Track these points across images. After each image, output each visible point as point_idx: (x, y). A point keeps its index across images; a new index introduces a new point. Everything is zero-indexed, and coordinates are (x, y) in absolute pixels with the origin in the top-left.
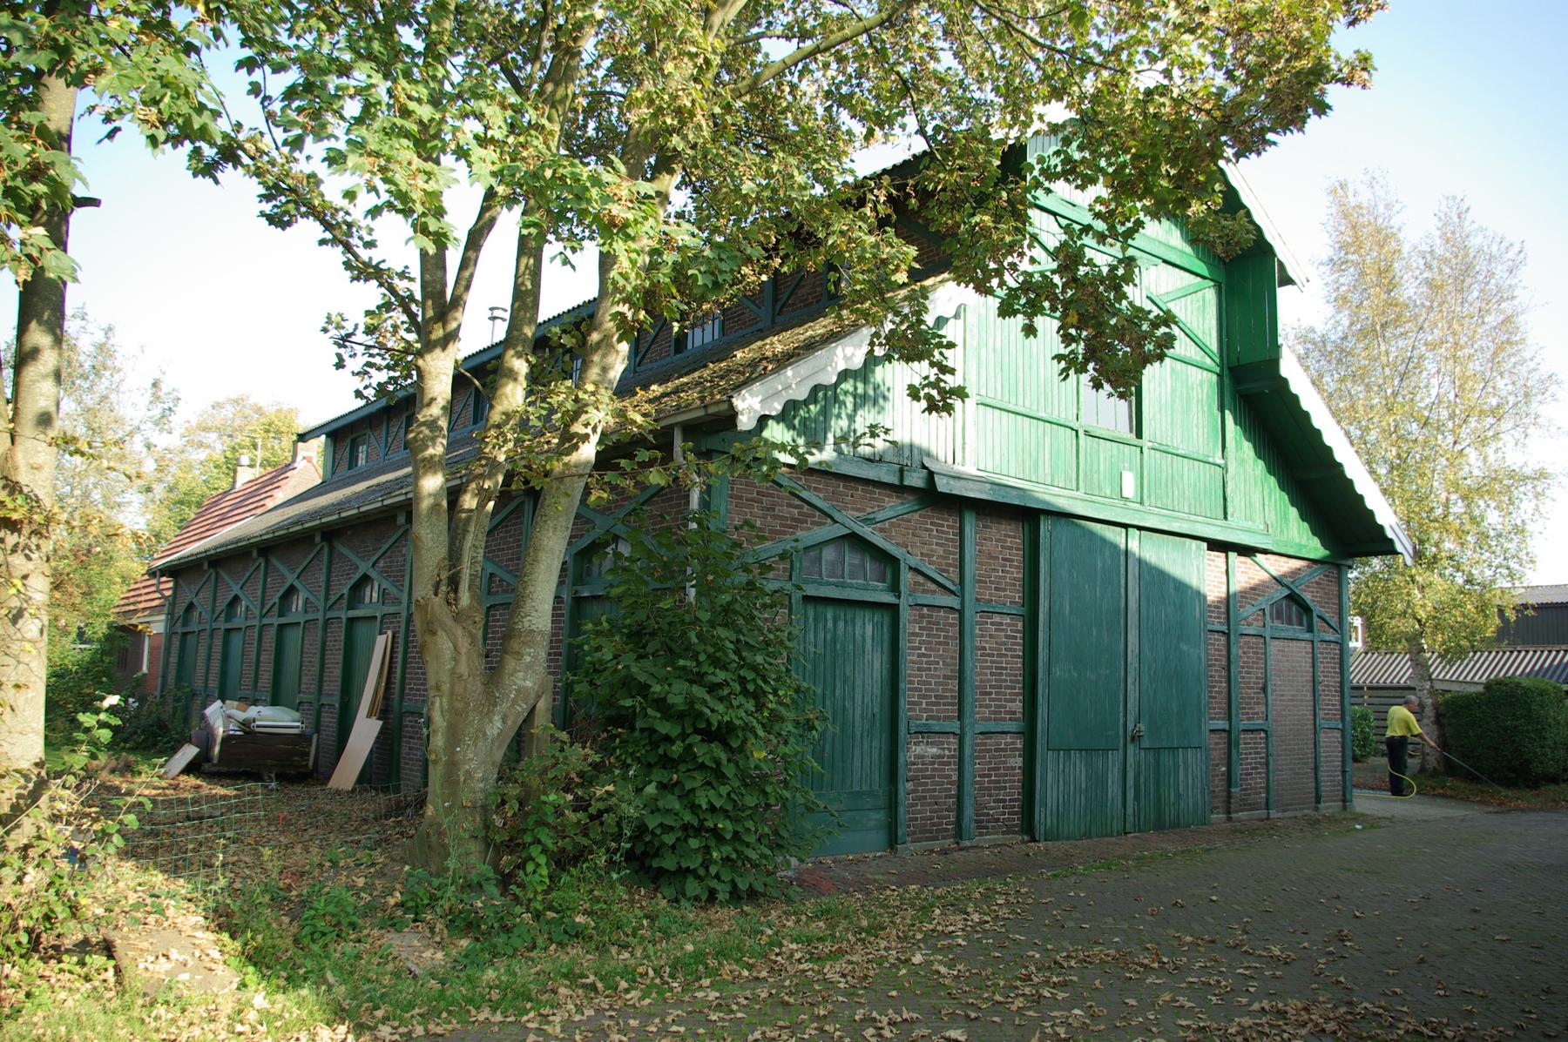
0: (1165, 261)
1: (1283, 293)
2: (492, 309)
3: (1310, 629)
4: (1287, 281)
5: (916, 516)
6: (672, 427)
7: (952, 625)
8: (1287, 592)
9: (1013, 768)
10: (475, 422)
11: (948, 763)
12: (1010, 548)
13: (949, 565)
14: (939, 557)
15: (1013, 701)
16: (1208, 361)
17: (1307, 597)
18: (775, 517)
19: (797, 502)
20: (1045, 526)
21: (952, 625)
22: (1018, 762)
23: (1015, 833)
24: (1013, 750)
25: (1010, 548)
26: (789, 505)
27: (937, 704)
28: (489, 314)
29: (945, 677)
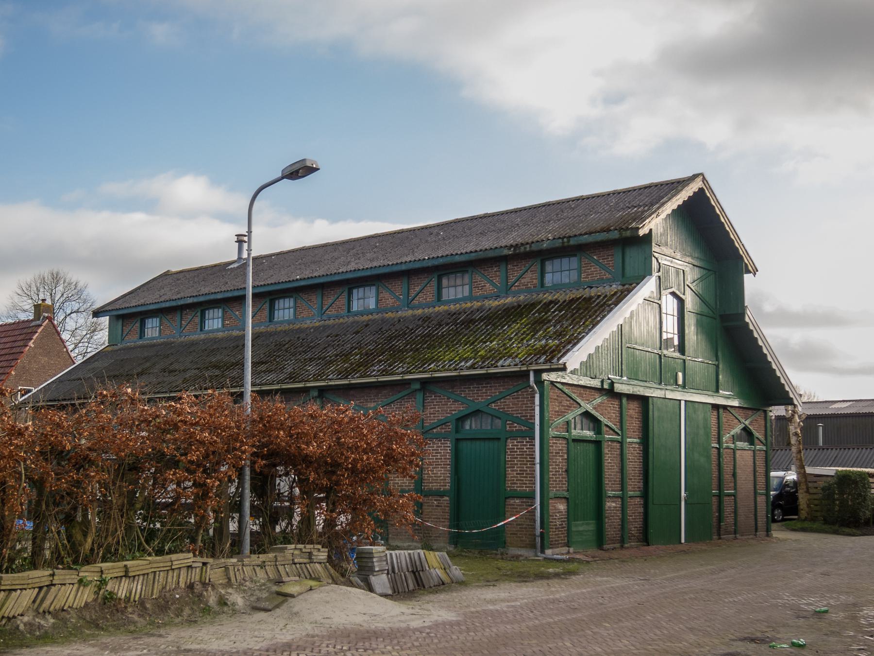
1: (747, 278)
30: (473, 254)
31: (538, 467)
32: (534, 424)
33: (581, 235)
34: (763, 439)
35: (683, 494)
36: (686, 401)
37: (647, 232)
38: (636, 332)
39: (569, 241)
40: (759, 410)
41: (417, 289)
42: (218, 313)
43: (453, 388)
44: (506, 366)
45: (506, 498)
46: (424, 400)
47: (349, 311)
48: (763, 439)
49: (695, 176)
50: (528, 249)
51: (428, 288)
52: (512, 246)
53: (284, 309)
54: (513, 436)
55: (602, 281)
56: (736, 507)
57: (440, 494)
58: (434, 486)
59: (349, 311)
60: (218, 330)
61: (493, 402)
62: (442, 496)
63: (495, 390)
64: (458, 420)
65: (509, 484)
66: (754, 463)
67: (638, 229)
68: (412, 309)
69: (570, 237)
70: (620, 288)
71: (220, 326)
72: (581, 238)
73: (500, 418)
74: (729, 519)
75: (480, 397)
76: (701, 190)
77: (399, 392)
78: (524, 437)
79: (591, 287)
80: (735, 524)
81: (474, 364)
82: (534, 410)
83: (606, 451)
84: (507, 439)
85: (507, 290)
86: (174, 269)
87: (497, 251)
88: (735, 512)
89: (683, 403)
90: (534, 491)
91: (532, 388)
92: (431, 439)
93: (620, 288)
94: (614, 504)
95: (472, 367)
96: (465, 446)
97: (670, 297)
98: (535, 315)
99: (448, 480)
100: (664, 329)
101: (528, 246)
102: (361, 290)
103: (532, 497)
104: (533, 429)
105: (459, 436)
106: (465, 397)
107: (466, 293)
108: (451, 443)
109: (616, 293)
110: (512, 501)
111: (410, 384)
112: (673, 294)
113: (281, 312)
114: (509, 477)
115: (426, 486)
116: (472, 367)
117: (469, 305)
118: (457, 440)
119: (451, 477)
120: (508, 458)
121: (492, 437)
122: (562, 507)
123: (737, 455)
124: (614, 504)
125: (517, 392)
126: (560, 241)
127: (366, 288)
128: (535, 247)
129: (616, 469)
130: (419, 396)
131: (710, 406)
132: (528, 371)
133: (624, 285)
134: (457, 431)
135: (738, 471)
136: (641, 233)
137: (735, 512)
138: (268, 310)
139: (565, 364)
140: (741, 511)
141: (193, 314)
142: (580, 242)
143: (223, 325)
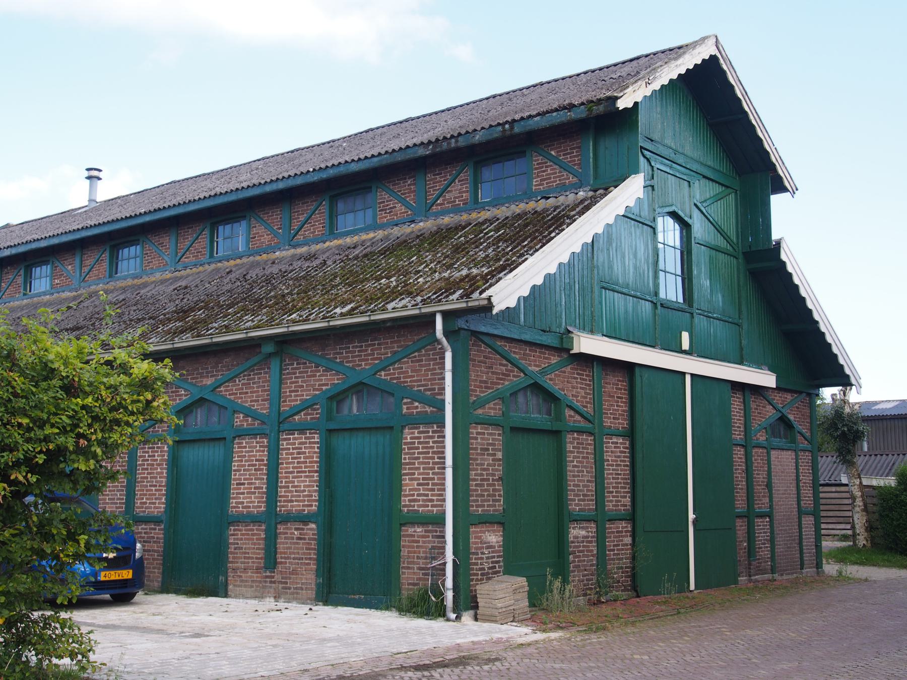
0: (704, 177)
1: (777, 201)
2: (88, 170)
3: (793, 441)
4: (779, 187)
5: (568, 369)
6: (433, 315)
7: (590, 444)
8: (780, 415)
9: (627, 545)
10: (110, 276)
11: (591, 542)
12: (621, 389)
13: (587, 403)
14: (582, 397)
15: (625, 497)
16: (729, 247)
17: (791, 417)
18: (493, 373)
19: (505, 362)
20: (637, 370)
21: (590, 444)
22: (628, 540)
23: (628, 590)
24: (626, 532)
25: (621, 389)
26: (501, 365)
27: (584, 500)
28: (86, 174)
29: (588, 481)
30: (375, 159)
31: (449, 473)
32: (443, 401)
33: (530, 117)
34: (808, 435)
35: (691, 516)
36: (692, 375)
37: (630, 105)
38: (617, 268)
39: (512, 128)
40: (801, 393)
41: (302, 218)
42: (46, 270)
43: (323, 350)
44: (400, 308)
45: (402, 525)
46: (281, 370)
47: (211, 256)
48: (808, 435)
49: (703, 39)
50: (453, 145)
51: (317, 216)
52: (430, 142)
53: (129, 259)
54: (414, 422)
55: (563, 188)
56: (772, 532)
57: (304, 519)
58: (295, 507)
59: (211, 256)
60: (45, 294)
61: (384, 369)
62: (306, 523)
63: (385, 349)
64: (331, 398)
65: (405, 501)
66: (797, 469)
67: (617, 98)
68: (294, 247)
69: (514, 121)
70: (591, 194)
71: (48, 288)
72: (530, 122)
73: (393, 395)
74: (764, 552)
75: (362, 361)
76: (713, 58)
77: (247, 359)
78: (429, 423)
79: (548, 198)
80: (772, 558)
81: (353, 309)
82: (444, 379)
83: (570, 447)
84: (403, 427)
85: (427, 211)
86: (15, 222)
87: (409, 151)
88: (772, 540)
89: (688, 378)
90: (444, 512)
91: (439, 342)
92: (291, 431)
93: (591, 194)
94: (583, 533)
95: (350, 313)
96: (342, 443)
97: (670, 221)
98: (460, 238)
99: (315, 496)
100: (661, 265)
101: (453, 140)
102: (228, 227)
103: (441, 522)
104: (442, 409)
105: (332, 426)
106: (341, 363)
107: (369, 221)
108: (320, 438)
109: (582, 201)
110: (411, 530)
111: (259, 346)
112: (674, 215)
113: (125, 262)
114: (406, 490)
115: (283, 507)
116: (350, 313)
117: (371, 235)
118: (330, 431)
119: (319, 491)
120: (405, 458)
121: (379, 425)
122: (494, 538)
123: (773, 459)
124: (583, 533)
125: (419, 350)
126: (500, 128)
127: (235, 225)
128: (462, 142)
129: (587, 476)
130: (275, 364)
131: (729, 385)
132: (433, 315)
133: (595, 191)
134: (330, 418)
135: (775, 480)
136: (621, 104)
137: (772, 540)
138: (108, 261)
139: (489, 299)
140: (780, 540)
141: (16, 271)
142: (528, 128)
143: (52, 287)
